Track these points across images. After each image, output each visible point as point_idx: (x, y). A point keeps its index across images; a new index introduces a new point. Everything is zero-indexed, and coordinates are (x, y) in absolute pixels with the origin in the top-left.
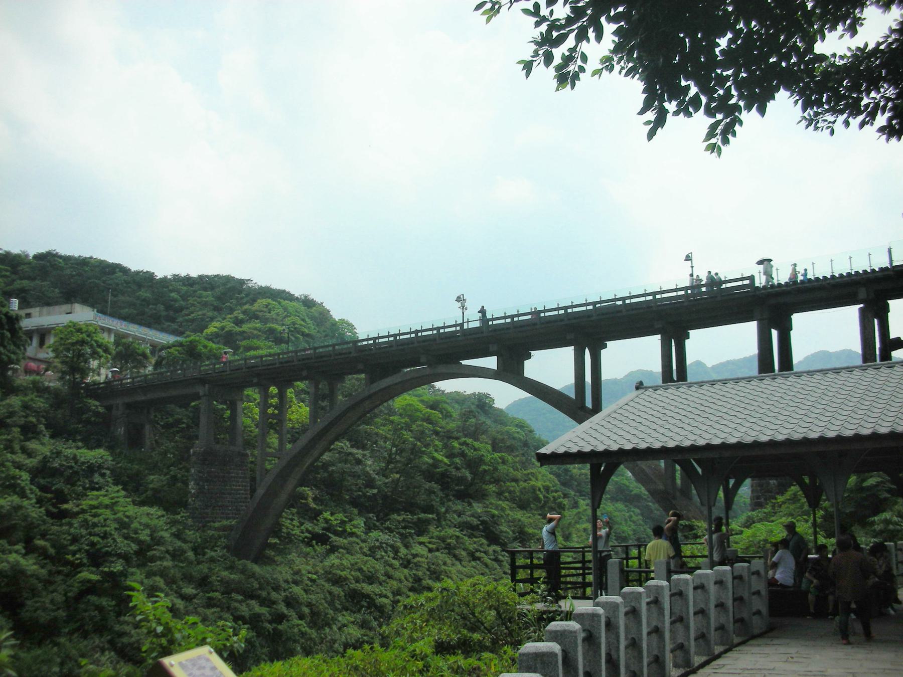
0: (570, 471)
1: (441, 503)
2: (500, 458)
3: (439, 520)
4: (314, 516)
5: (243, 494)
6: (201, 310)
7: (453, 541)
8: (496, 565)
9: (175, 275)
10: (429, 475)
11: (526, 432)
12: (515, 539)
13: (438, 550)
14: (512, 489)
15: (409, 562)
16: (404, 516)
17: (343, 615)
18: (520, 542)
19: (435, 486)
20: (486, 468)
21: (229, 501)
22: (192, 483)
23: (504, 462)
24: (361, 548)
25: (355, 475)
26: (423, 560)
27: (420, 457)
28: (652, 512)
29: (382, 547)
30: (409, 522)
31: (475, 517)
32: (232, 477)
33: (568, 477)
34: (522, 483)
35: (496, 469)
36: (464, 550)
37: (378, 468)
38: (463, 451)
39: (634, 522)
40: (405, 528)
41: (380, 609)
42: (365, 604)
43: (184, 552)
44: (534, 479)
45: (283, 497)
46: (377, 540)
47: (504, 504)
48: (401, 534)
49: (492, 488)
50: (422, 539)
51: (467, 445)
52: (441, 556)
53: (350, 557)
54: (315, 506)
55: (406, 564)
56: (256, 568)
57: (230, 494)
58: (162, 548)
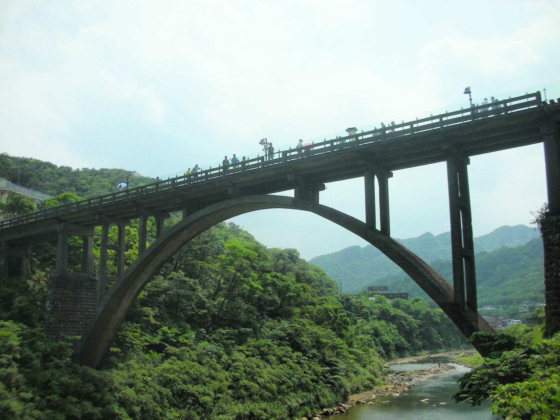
0: (350, 300)
1: (258, 321)
2: (301, 287)
3: (255, 333)
4: (154, 330)
5: (92, 312)
6: (100, 190)
7: (265, 349)
8: (298, 367)
9: (84, 169)
10: (248, 298)
11: (321, 274)
12: (313, 347)
13: (253, 356)
14: (311, 310)
15: (229, 365)
16: (229, 331)
17: (171, 411)
18: (316, 349)
19: (254, 308)
20: (291, 294)
21: (79, 318)
22: (48, 302)
23: (304, 290)
24: (190, 355)
25: (189, 298)
26: (241, 364)
27: (241, 285)
28: (404, 326)
29: (208, 354)
30: (232, 335)
31: (282, 331)
32: (82, 298)
33: (349, 304)
34: (318, 307)
35: (299, 295)
36: (274, 355)
37: (208, 293)
38: (274, 282)
39: (393, 334)
40: (227, 339)
41: (203, 405)
42: (190, 401)
43: (32, 359)
44: (326, 303)
45: (120, 313)
46: (205, 349)
47: (305, 321)
48: (225, 345)
49: (297, 310)
50: (241, 348)
51: (277, 278)
52: (256, 360)
53: (179, 362)
54: (155, 322)
55: (227, 367)
56: (94, 372)
57: (80, 311)
58: (10, 357)
